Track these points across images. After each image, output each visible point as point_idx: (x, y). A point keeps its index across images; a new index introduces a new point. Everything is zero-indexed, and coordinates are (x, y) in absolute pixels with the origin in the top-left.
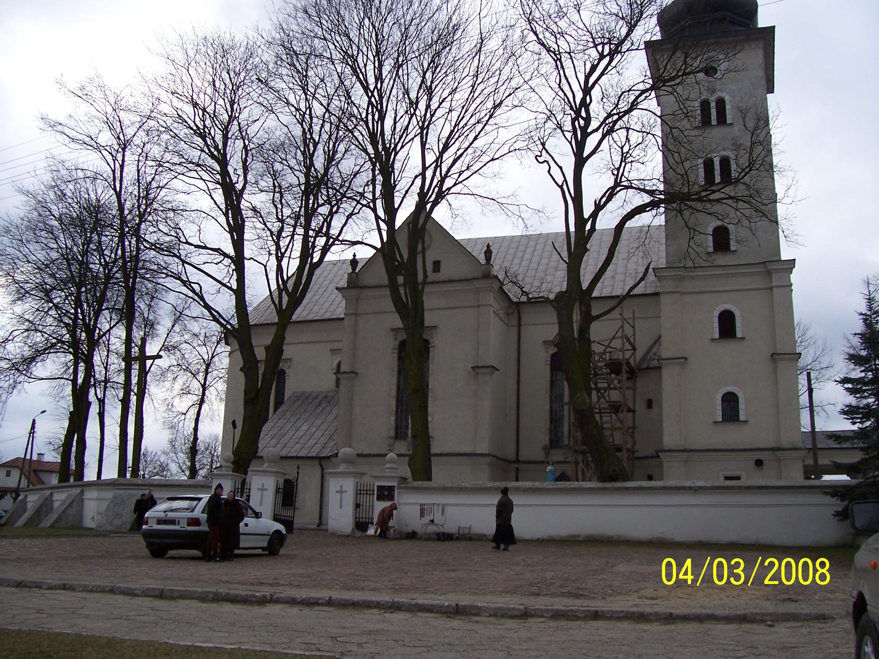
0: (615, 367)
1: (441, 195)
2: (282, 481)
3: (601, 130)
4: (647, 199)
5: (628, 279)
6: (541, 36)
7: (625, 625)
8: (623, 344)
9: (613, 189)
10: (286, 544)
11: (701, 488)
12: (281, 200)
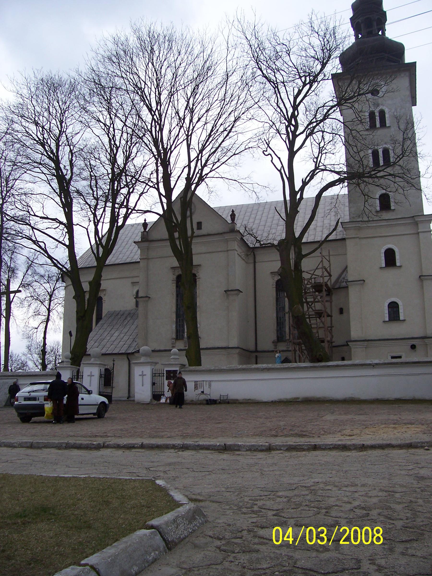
0: (318, 288)
1: (201, 179)
2: (103, 370)
3: (305, 133)
4: (337, 177)
5: (325, 230)
6: (265, 72)
7: (334, 453)
8: (323, 273)
9: (314, 171)
10: (109, 411)
11: (377, 364)
12: (96, 186)
